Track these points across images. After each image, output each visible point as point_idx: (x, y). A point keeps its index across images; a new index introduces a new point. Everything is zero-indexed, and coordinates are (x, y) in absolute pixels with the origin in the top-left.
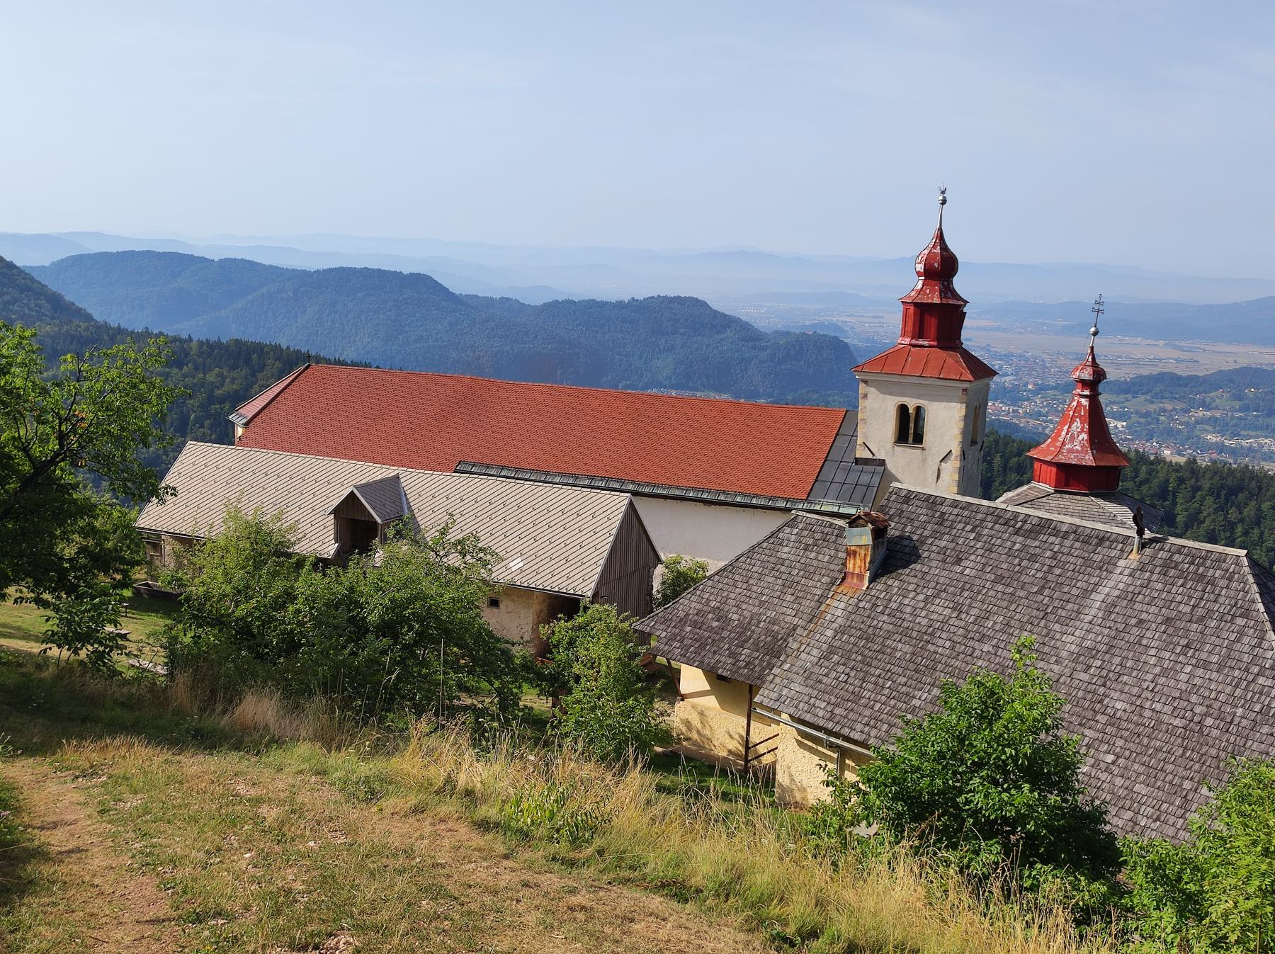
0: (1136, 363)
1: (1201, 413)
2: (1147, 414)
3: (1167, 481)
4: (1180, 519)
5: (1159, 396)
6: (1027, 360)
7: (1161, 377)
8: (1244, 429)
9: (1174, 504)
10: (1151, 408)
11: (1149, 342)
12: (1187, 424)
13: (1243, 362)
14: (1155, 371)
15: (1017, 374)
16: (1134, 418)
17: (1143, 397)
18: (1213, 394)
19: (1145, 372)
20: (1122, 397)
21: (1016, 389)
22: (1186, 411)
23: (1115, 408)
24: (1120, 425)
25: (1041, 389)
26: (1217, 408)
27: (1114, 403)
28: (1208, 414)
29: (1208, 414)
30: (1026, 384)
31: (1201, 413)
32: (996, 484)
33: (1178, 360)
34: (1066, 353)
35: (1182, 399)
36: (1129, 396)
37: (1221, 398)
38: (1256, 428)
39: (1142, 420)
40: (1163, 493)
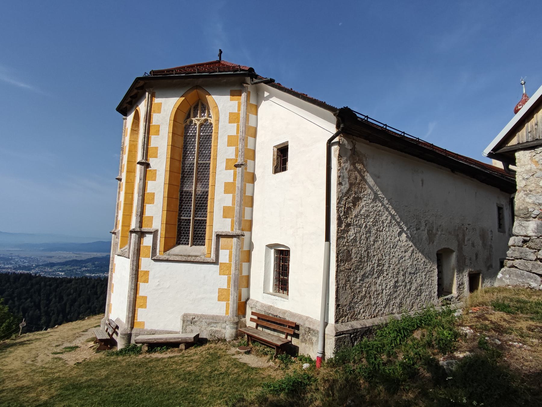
0: (65, 258)
1: (84, 269)
2: (70, 270)
3: (94, 283)
4: (99, 293)
5: (73, 265)
6: (32, 258)
7: (73, 261)
8: (96, 272)
9: (97, 289)
10: (71, 268)
11: (68, 252)
12: (81, 272)
13: (92, 256)
14: (71, 259)
15: (29, 262)
16: (66, 271)
17: (68, 266)
18: (87, 264)
19: (68, 260)
20: (63, 266)
21: (29, 266)
22: (80, 269)
23: (61, 269)
24: (62, 273)
25: (37, 266)
26: (88, 267)
27: (60, 268)
28: (86, 269)
29: (86, 269)
30: (32, 265)
31: (84, 269)
32: (43, 290)
33: (76, 257)
34: (44, 256)
35: (79, 266)
36: (65, 266)
37: (89, 264)
38: (99, 271)
39: (69, 272)
40: (94, 286)
